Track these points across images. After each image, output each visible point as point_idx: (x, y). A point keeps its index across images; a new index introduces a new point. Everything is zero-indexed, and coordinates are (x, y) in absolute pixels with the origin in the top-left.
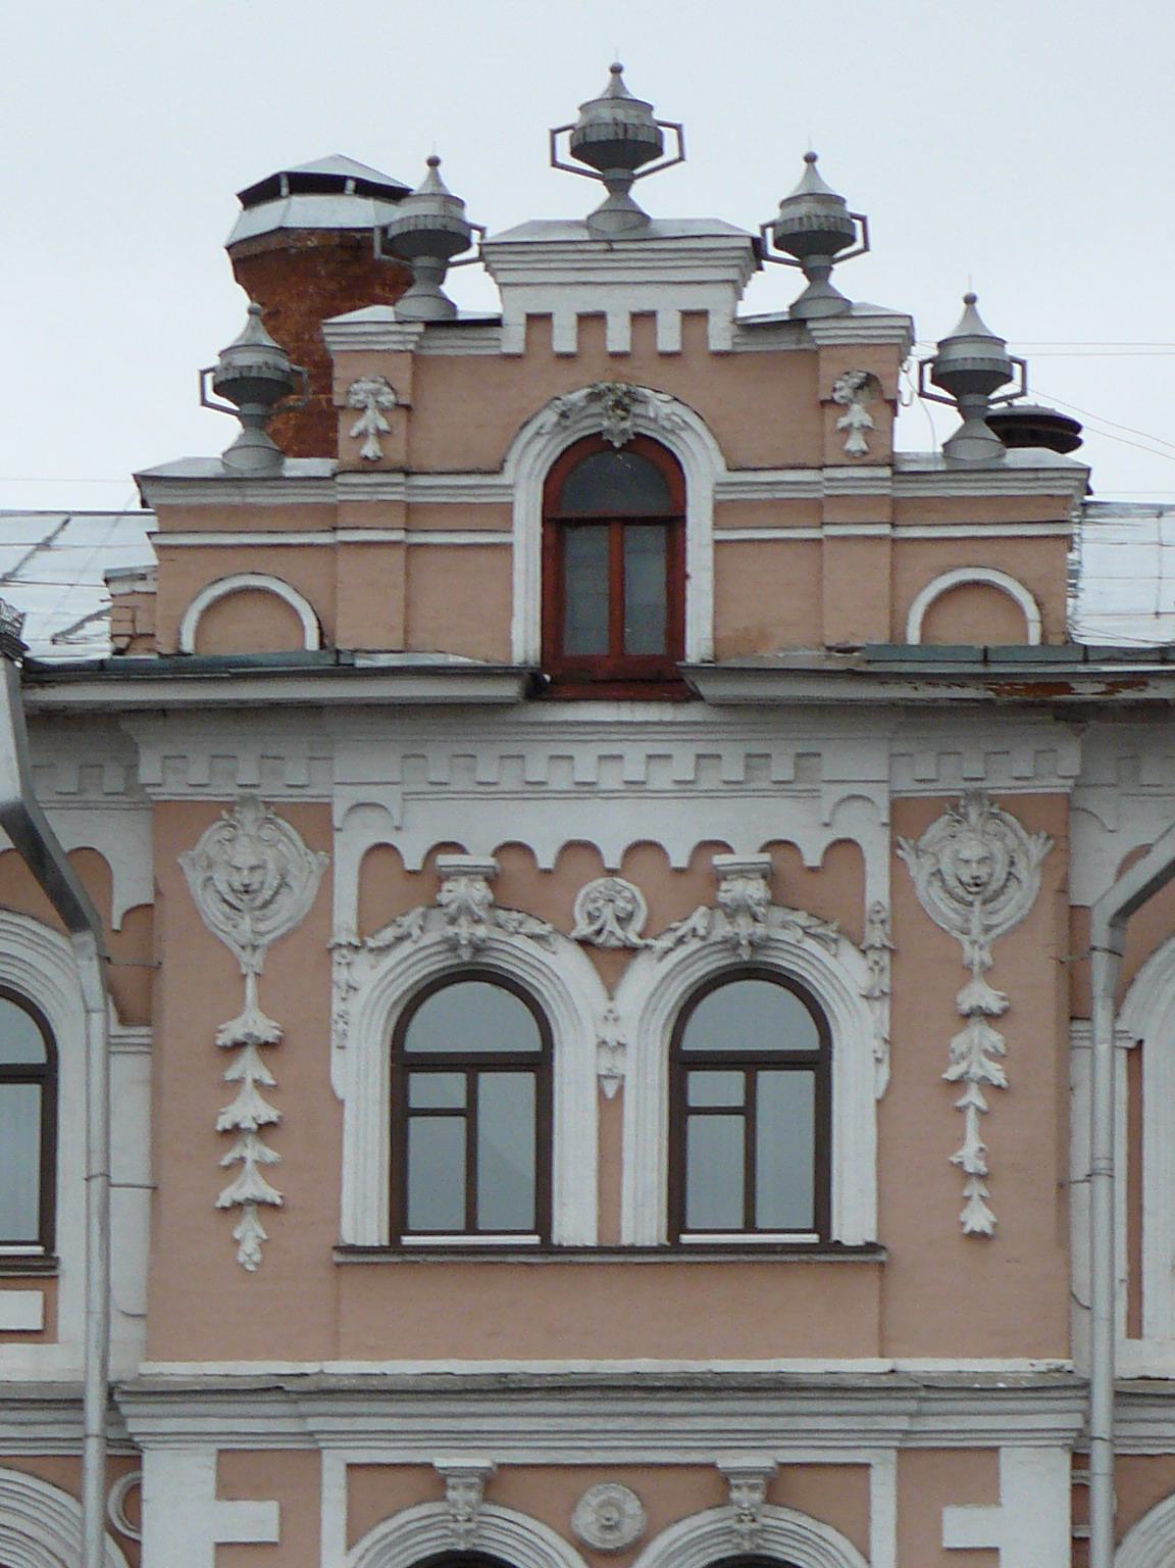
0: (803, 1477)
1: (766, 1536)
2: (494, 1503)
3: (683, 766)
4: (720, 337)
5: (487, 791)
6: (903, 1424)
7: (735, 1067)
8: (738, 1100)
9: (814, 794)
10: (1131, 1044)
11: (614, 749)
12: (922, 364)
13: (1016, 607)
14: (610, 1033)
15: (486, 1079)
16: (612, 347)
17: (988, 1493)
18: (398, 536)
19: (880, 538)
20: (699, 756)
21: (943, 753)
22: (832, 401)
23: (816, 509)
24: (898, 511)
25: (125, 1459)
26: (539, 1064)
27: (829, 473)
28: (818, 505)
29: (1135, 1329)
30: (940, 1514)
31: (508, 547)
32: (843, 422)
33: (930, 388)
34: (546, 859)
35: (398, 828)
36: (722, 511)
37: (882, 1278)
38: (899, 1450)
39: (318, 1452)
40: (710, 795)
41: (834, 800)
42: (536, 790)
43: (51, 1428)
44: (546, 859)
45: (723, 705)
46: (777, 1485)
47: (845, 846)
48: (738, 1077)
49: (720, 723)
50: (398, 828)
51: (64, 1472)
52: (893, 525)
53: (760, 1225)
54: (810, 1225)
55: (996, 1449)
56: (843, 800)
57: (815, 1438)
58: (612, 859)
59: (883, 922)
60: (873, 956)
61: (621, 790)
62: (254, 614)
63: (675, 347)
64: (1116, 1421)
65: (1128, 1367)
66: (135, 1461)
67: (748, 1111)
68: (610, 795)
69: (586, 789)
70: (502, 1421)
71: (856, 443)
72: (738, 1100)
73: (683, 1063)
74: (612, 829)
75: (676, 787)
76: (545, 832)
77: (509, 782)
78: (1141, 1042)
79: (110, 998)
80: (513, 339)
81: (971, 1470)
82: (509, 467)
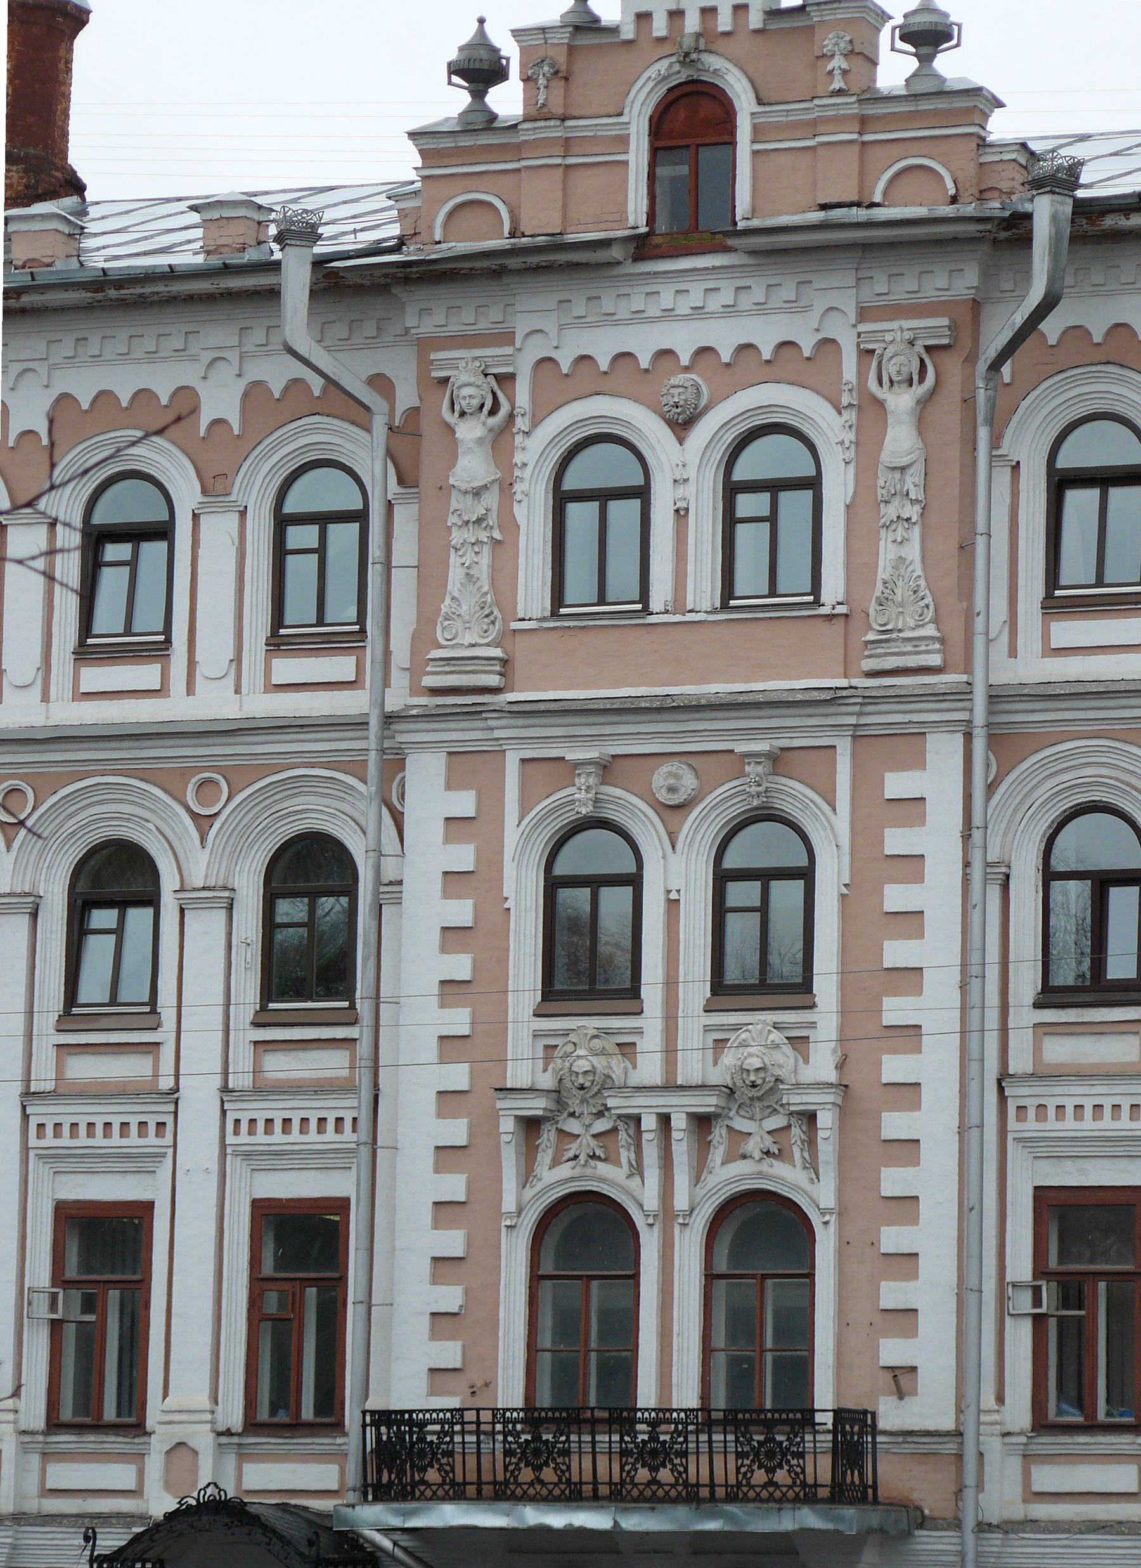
0: (620, 763)
1: (769, 794)
2: (607, 784)
3: (726, 296)
4: (755, 20)
5: (610, 319)
6: (852, 720)
7: (761, 490)
8: (766, 512)
9: (808, 307)
10: (1014, 463)
11: (683, 287)
12: (894, 29)
13: (489, 205)
14: (686, 473)
15: (783, 496)
16: (656, 34)
17: (918, 762)
18: (559, 161)
19: (851, 142)
20: (738, 288)
21: (803, 283)
22: (824, 56)
23: (813, 127)
24: (864, 123)
25: (394, 764)
26: (642, 493)
27: (817, 102)
28: (814, 122)
29: (1013, 652)
30: (471, 789)
31: (626, 163)
32: (830, 67)
33: (900, 44)
34: (644, 362)
35: (556, 347)
36: (758, 133)
37: (846, 622)
38: (854, 737)
39: (504, 751)
40: (778, 310)
41: (822, 310)
42: (639, 317)
43: (347, 743)
44: (644, 362)
45: (752, 253)
46: (777, 760)
47: (829, 343)
48: (766, 497)
49: (741, 266)
50: (556, 347)
51: (357, 769)
52: (861, 134)
53: (609, 600)
54: (809, 590)
55: (924, 733)
56: (824, 314)
57: (800, 731)
58: (685, 360)
59: (850, 390)
60: (846, 415)
61: (690, 312)
62: (472, 217)
63: (728, 28)
64: (990, 713)
65: (1001, 677)
66: (401, 764)
67: (772, 519)
68: (712, 315)
69: (669, 314)
70: (1135, 711)
71: (838, 84)
72: (766, 512)
73: (732, 490)
74: (684, 340)
75: (694, 312)
76: (644, 344)
77: (653, 312)
78: (1018, 463)
79: (390, 465)
80: (628, 33)
81: (907, 745)
82: (626, 111)
